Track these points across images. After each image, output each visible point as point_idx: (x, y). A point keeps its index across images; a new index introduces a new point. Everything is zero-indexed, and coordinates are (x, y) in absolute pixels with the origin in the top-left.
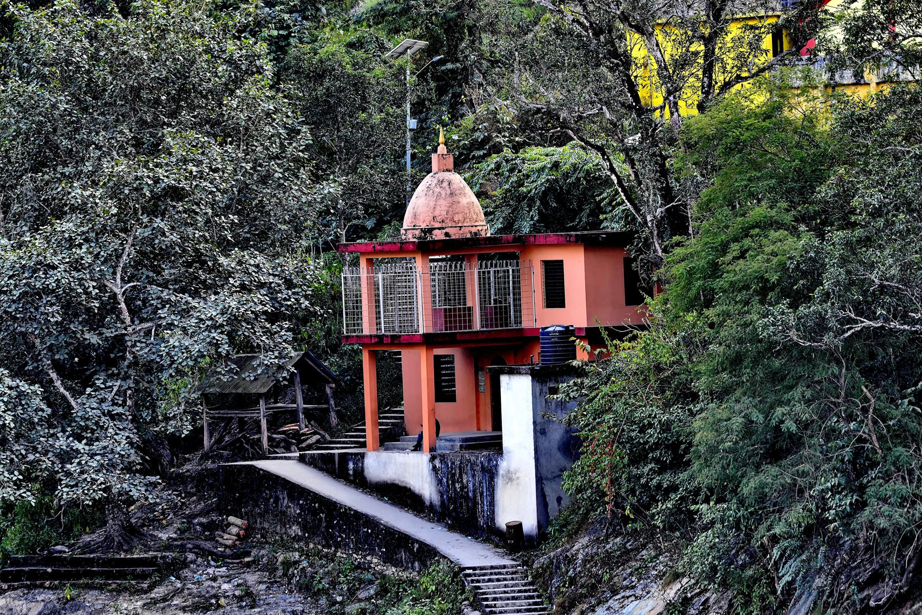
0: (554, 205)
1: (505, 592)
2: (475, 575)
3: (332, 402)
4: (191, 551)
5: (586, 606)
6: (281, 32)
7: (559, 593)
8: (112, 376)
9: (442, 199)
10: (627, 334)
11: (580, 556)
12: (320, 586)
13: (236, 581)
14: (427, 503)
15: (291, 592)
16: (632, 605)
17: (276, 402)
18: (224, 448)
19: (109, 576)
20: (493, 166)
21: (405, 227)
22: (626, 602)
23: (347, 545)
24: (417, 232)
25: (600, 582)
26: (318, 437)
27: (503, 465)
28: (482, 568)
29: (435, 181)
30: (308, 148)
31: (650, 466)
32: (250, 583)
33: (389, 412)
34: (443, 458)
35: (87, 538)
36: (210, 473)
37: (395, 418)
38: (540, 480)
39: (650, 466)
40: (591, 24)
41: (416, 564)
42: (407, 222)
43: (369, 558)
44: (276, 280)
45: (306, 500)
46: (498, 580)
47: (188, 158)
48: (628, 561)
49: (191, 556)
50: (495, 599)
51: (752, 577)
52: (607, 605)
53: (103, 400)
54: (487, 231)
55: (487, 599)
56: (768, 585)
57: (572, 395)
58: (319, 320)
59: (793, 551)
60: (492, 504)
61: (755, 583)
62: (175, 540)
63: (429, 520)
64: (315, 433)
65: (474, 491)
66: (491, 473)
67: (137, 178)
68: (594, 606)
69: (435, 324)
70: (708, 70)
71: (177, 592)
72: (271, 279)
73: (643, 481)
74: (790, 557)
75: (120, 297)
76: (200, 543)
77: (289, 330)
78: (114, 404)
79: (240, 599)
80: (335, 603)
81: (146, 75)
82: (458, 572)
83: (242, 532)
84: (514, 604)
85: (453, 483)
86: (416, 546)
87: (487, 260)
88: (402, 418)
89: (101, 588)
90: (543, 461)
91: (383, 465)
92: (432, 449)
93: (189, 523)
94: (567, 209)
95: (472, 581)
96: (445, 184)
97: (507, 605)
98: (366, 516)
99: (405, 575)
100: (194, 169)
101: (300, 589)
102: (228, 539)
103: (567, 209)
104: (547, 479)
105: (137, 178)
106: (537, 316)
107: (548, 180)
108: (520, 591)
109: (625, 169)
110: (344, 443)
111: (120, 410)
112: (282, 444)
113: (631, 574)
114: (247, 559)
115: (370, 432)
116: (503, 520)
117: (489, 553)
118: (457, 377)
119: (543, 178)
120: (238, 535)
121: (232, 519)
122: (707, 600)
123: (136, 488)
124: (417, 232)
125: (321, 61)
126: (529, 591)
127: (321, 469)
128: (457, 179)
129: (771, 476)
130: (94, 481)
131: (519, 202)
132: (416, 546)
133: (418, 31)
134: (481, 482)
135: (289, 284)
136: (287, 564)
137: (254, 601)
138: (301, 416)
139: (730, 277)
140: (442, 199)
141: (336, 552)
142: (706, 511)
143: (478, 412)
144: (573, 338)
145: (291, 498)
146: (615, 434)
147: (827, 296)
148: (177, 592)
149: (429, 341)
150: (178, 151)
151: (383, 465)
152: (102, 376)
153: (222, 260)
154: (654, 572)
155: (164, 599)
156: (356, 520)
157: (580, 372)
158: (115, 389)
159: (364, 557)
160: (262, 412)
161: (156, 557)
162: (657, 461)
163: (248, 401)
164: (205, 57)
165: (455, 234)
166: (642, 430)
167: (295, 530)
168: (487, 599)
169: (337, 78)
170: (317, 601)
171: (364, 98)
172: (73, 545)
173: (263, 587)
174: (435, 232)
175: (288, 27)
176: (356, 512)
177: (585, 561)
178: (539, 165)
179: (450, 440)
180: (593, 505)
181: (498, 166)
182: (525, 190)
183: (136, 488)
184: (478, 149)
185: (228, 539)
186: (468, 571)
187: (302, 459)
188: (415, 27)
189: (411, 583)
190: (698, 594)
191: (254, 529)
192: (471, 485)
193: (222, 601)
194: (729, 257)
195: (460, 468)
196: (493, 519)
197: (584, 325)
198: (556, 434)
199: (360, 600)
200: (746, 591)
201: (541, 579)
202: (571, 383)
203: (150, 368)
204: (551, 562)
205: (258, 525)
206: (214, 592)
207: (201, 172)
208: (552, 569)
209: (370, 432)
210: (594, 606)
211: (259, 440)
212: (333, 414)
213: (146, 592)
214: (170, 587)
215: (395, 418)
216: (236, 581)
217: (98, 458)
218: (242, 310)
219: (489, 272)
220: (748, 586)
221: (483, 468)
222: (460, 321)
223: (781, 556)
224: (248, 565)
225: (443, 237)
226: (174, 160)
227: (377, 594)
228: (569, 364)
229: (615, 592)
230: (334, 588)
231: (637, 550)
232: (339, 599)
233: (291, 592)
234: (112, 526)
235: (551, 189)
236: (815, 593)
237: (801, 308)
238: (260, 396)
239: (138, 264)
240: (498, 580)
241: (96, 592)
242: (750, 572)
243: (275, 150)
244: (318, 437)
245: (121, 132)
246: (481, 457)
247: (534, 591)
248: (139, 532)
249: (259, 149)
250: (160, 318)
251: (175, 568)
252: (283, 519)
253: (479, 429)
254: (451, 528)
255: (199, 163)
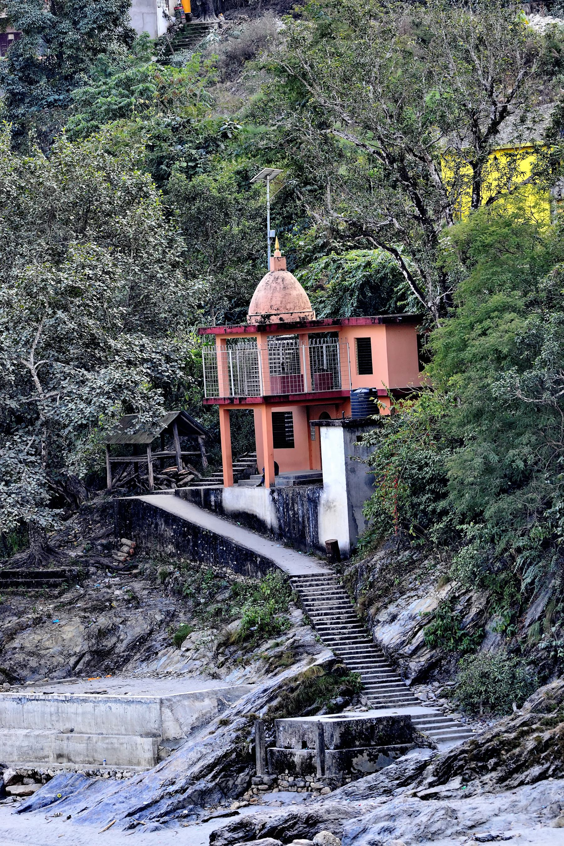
0: (370, 294)
1: (322, 594)
2: (299, 581)
3: (203, 449)
4: (93, 565)
5: (381, 604)
6: (190, 164)
7: (361, 594)
8: (29, 433)
9: (278, 292)
10: (408, 394)
11: (378, 566)
12: (188, 591)
13: (125, 589)
14: (269, 527)
15: (167, 596)
16: (415, 603)
17: (163, 450)
18: (122, 486)
19: (28, 585)
20: (323, 265)
21: (250, 314)
22: (411, 601)
23: (208, 559)
24: (259, 318)
25: (392, 585)
26: (192, 476)
27: (324, 496)
28: (305, 576)
29: (272, 278)
30: (183, 254)
31: (427, 496)
32: (136, 590)
33: (247, 456)
34: (280, 492)
35: (18, 556)
36: (111, 505)
37: (251, 461)
38: (351, 507)
39: (427, 496)
40: (387, 155)
41: (259, 574)
42: (251, 311)
43: (224, 569)
44: (158, 356)
45: (178, 525)
46: (317, 585)
47: (85, 264)
48: (413, 569)
49: (92, 569)
50: (313, 600)
51: (504, 579)
52: (396, 603)
53: (20, 451)
54: (312, 316)
55: (307, 600)
56: (515, 586)
57: (371, 442)
58: (180, 388)
59: (534, 559)
60: (316, 526)
61: (506, 584)
62: (82, 557)
63: (270, 539)
64: (190, 473)
65: (303, 517)
66: (314, 502)
67: (43, 280)
68: (386, 604)
69: (272, 390)
70: (477, 189)
71: (80, 597)
72: (153, 355)
73: (422, 507)
74: (531, 564)
75: (33, 372)
76: (101, 560)
77: (161, 395)
78: (28, 454)
79: (128, 601)
80: (199, 604)
81: (58, 200)
82: (288, 579)
83: (131, 551)
84: (328, 604)
85: (288, 511)
86: (259, 559)
87: (320, 338)
88: (256, 461)
89: (23, 595)
90: (353, 493)
91: (236, 497)
92: (272, 485)
93: (92, 544)
94: (378, 299)
95: (297, 586)
96: (280, 281)
97: (322, 604)
98: (222, 537)
99: (251, 582)
100: (91, 272)
101: (174, 593)
102: (121, 556)
103: (378, 299)
104: (356, 507)
105: (43, 280)
106: (352, 381)
107: (364, 276)
108: (333, 593)
109: (414, 267)
110: (211, 480)
111: (33, 458)
112: (165, 482)
113: (415, 579)
114: (135, 571)
115: (227, 471)
116: (325, 537)
117: (312, 564)
118: (295, 429)
119: (360, 274)
120: (128, 553)
121: (124, 540)
122: (471, 597)
123: (44, 519)
124: (259, 318)
125: (194, 187)
126: (340, 593)
127: (191, 501)
128: (288, 275)
129: (507, 503)
130: (10, 513)
131: (344, 292)
132: (259, 559)
133: (286, 161)
134: (308, 510)
135: (168, 360)
136: (165, 575)
137: (138, 603)
138: (180, 461)
139: (474, 350)
140: (278, 292)
141: (200, 564)
142: (470, 529)
143: (311, 456)
144: (372, 398)
145: (167, 523)
146: (399, 472)
147: (544, 363)
148: (80, 597)
149: (268, 401)
150: (78, 258)
151: (236, 497)
152: (21, 432)
153: (112, 342)
154: (432, 578)
155: (70, 603)
156: (214, 540)
157: (379, 424)
158: (30, 443)
159: (221, 568)
160: (149, 458)
161: (64, 571)
162: (432, 492)
163: (139, 450)
164: (104, 185)
165: (288, 319)
166: (421, 468)
167: (170, 548)
168: (307, 600)
169: (206, 200)
170: (186, 602)
171: (226, 214)
172: (7, 561)
173: (146, 592)
174: (272, 317)
175: (195, 160)
176: (214, 534)
177: (381, 570)
178: (356, 264)
179: (286, 478)
180: (387, 526)
181: (327, 265)
182: (347, 283)
183: (44, 519)
184: (319, 252)
185: (121, 556)
186: (294, 579)
187: (177, 494)
188: (283, 158)
189: (256, 588)
190: (464, 594)
191: (140, 548)
192: (300, 512)
193: (114, 604)
194: (474, 334)
195: (292, 499)
196: (317, 538)
197: (387, 386)
198: (363, 472)
199: (218, 602)
200: (499, 590)
201: (349, 584)
202: (372, 432)
203: (53, 425)
204: (357, 571)
205: (143, 545)
206: (108, 597)
207: (96, 274)
208: (357, 575)
209: (227, 471)
210: (386, 604)
211: (147, 479)
212: (204, 459)
213: (57, 598)
214: (75, 594)
215: (251, 461)
216: (125, 589)
217: (13, 496)
218: (124, 380)
219: (322, 347)
220: (501, 587)
221: (309, 499)
222: (292, 386)
223: (524, 563)
224: (136, 576)
225: (278, 322)
226: (75, 265)
227: (230, 598)
228: (370, 419)
229: (402, 593)
230: (199, 593)
231: (421, 560)
232: (202, 601)
233: (167, 596)
234: (34, 548)
235: (367, 283)
236: (550, 591)
237: (525, 373)
238: (147, 445)
239: (48, 345)
240: (317, 585)
241: (20, 598)
242: (503, 576)
243: (157, 255)
244: (192, 476)
245: (39, 244)
246: (307, 490)
247: (344, 593)
248: (55, 552)
249: (145, 255)
250: (63, 388)
251: (79, 578)
252: (161, 540)
253: (311, 469)
254: (287, 546)
255: (94, 268)
